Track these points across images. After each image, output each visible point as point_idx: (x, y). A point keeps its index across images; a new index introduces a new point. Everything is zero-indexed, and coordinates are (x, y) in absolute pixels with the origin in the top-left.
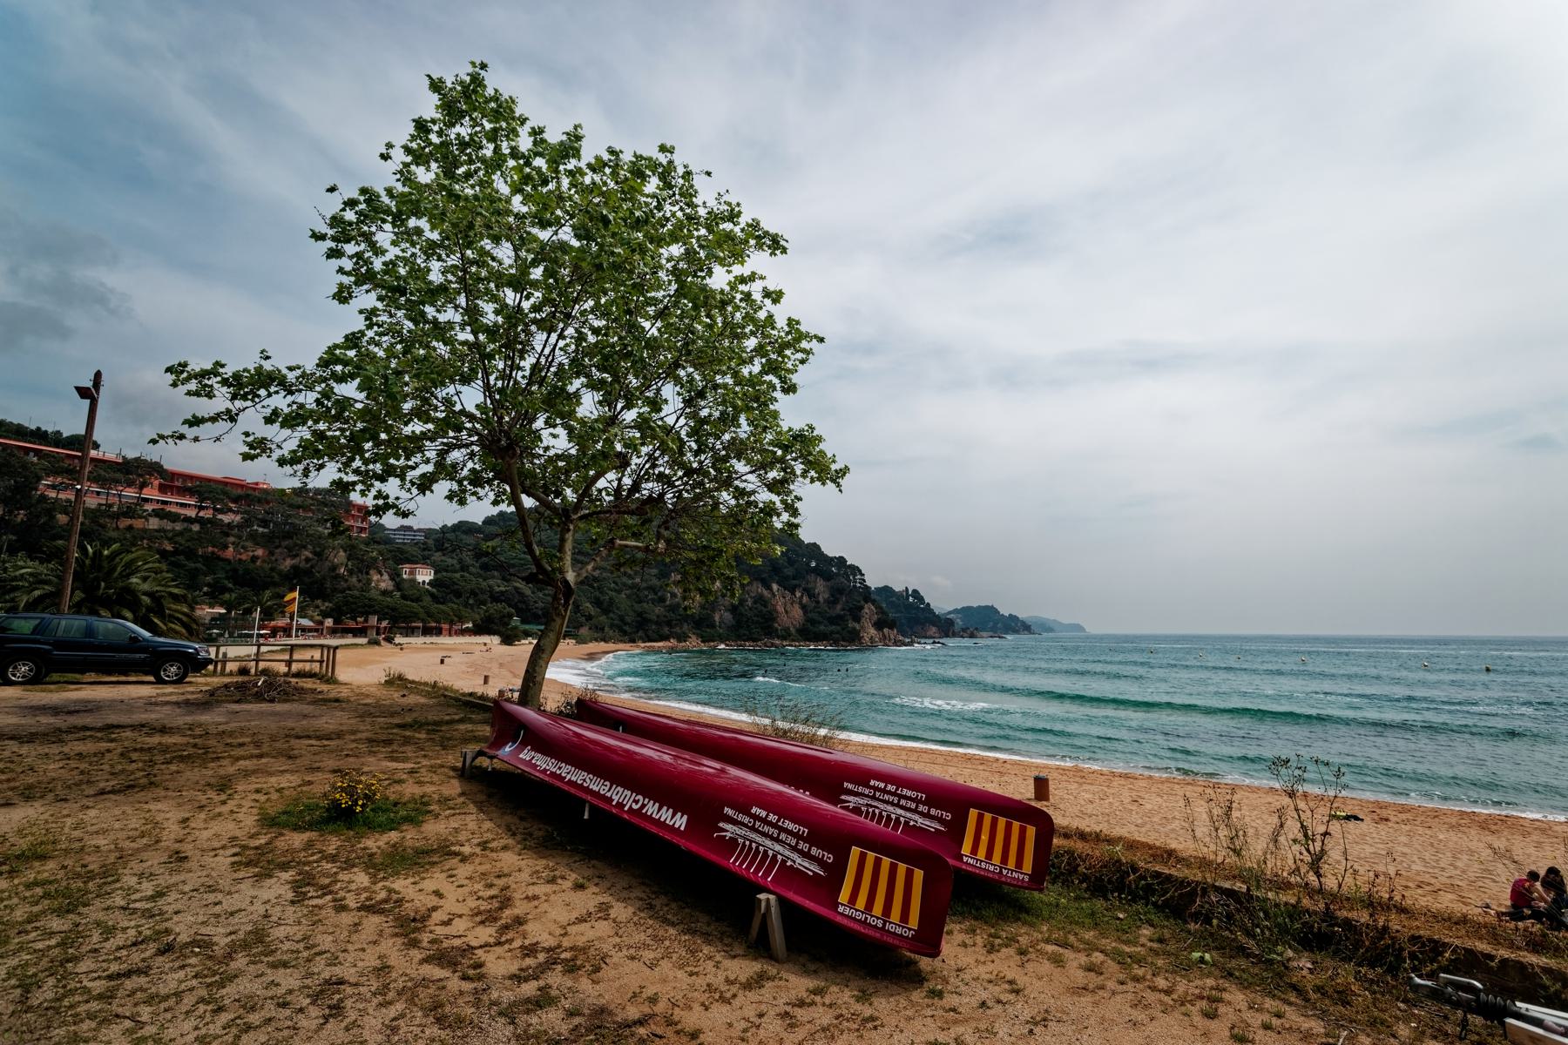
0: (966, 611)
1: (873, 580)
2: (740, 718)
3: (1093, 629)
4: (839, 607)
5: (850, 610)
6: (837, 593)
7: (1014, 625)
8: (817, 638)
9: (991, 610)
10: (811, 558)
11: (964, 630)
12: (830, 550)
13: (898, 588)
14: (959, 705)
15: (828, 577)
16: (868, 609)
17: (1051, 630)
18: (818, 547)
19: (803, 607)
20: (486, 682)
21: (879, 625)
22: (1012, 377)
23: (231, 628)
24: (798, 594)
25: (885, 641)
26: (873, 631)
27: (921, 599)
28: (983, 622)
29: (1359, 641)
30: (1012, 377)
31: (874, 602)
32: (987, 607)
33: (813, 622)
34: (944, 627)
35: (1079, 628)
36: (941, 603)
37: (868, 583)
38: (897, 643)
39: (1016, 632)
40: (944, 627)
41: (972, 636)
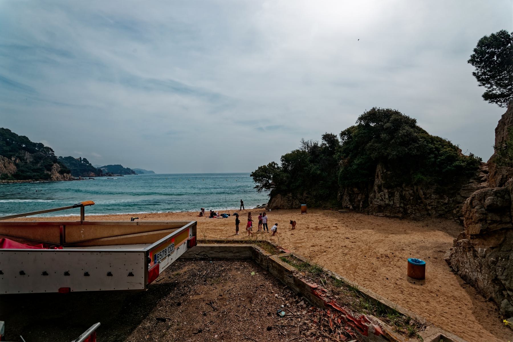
0: (109, 167)
1: (57, 154)
2: (57, 216)
3: (157, 172)
4: (39, 165)
5: (45, 166)
6: (37, 159)
7: (129, 172)
8: (26, 178)
9: (120, 166)
10: (23, 143)
11: (107, 174)
12: (33, 139)
13: (76, 157)
14: (123, 201)
15: (32, 151)
16: (55, 166)
17: (143, 173)
18: (27, 138)
19: (17, 165)
20: (242, 205)
21: (61, 172)
22: (130, 82)
23: (432, 148)
24: (13, 159)
25: (64, 179)
26: (58, 175)
27: (87, 162)
28: (116, 171)
29: (170, 175)
30: (130, 82)
31: (59, 163)
32: (118, 165)
33: (22, 171)
34: (99, 172)
35: (153, 172)
36: (96, 163)
37: (55, 155)
38: (70, 180)
39: (129, 174)
40: (99, 172)
41: (110, 176)
